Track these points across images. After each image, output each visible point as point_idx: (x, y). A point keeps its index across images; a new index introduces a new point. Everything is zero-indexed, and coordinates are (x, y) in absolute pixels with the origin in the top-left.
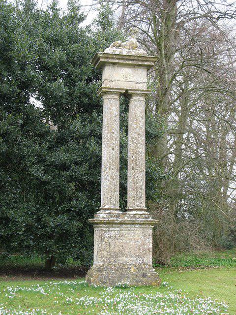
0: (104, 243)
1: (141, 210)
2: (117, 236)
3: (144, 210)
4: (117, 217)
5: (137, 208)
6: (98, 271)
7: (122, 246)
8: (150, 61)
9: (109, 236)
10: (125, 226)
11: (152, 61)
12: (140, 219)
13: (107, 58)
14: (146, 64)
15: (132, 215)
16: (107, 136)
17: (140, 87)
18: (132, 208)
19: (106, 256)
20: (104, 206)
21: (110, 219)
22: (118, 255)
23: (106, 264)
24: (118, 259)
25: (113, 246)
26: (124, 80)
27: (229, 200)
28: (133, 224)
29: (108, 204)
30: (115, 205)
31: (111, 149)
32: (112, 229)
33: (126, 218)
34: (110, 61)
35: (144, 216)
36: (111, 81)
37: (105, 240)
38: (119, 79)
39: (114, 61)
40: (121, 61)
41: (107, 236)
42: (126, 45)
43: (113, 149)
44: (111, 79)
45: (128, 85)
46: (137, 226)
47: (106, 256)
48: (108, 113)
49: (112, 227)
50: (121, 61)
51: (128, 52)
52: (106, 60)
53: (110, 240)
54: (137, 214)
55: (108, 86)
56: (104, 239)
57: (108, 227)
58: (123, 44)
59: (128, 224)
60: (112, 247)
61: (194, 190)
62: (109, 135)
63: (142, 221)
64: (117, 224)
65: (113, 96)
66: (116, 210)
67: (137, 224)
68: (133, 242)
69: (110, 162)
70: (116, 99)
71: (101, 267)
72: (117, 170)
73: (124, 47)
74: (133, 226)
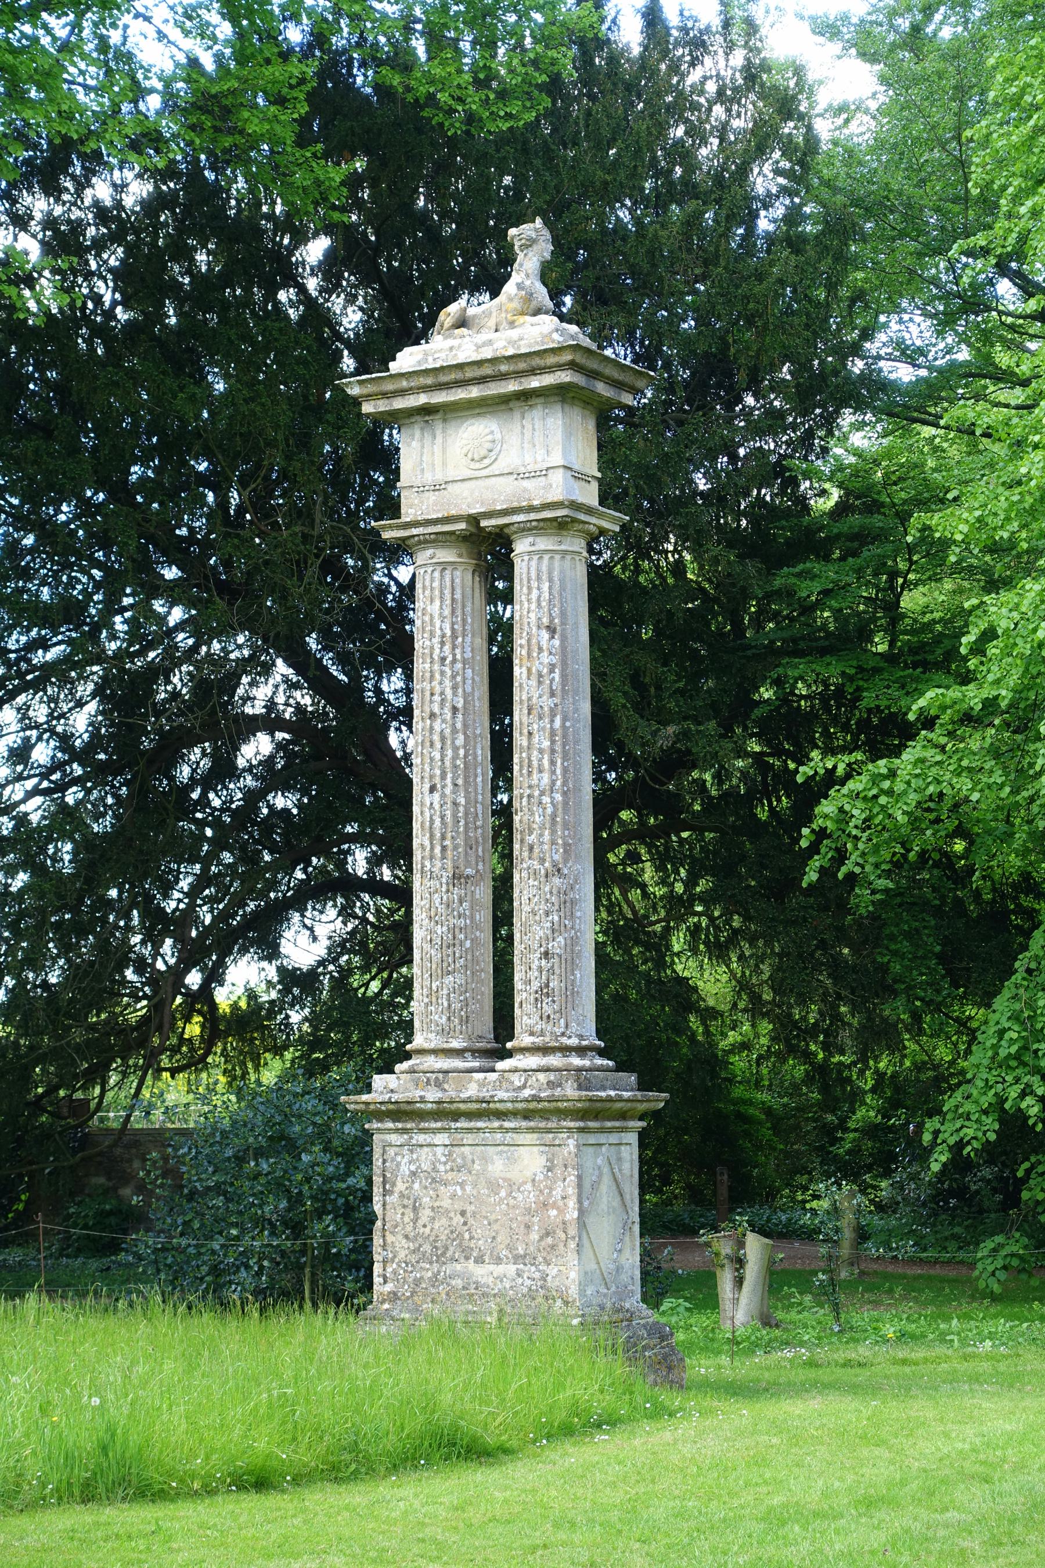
1: (581, 1051)
2: (442, 1168)
6: (928, 1529)
7: (463, 1213)
9: (413, 1168)
11: (560, 367)
17: (538, 492)
19: (402, 1255)
22: (449, 1254)
23: (406, 1290)
24: (449, 1269)
34: (399, 404)
35: (541, 1076)
36: (421, 490)
37: (400, 1186)
41: (405, 1170)
47: (402, 1255)
53: (416, 1186)
54: (515, 1070)
56: (394, 1185)
57: (405, 1131)
60: (425, 1214)
65: (429, 552)
68: (503, 1193)
70: (444, 566)
72: (457, 878)
74: (496, 1124)
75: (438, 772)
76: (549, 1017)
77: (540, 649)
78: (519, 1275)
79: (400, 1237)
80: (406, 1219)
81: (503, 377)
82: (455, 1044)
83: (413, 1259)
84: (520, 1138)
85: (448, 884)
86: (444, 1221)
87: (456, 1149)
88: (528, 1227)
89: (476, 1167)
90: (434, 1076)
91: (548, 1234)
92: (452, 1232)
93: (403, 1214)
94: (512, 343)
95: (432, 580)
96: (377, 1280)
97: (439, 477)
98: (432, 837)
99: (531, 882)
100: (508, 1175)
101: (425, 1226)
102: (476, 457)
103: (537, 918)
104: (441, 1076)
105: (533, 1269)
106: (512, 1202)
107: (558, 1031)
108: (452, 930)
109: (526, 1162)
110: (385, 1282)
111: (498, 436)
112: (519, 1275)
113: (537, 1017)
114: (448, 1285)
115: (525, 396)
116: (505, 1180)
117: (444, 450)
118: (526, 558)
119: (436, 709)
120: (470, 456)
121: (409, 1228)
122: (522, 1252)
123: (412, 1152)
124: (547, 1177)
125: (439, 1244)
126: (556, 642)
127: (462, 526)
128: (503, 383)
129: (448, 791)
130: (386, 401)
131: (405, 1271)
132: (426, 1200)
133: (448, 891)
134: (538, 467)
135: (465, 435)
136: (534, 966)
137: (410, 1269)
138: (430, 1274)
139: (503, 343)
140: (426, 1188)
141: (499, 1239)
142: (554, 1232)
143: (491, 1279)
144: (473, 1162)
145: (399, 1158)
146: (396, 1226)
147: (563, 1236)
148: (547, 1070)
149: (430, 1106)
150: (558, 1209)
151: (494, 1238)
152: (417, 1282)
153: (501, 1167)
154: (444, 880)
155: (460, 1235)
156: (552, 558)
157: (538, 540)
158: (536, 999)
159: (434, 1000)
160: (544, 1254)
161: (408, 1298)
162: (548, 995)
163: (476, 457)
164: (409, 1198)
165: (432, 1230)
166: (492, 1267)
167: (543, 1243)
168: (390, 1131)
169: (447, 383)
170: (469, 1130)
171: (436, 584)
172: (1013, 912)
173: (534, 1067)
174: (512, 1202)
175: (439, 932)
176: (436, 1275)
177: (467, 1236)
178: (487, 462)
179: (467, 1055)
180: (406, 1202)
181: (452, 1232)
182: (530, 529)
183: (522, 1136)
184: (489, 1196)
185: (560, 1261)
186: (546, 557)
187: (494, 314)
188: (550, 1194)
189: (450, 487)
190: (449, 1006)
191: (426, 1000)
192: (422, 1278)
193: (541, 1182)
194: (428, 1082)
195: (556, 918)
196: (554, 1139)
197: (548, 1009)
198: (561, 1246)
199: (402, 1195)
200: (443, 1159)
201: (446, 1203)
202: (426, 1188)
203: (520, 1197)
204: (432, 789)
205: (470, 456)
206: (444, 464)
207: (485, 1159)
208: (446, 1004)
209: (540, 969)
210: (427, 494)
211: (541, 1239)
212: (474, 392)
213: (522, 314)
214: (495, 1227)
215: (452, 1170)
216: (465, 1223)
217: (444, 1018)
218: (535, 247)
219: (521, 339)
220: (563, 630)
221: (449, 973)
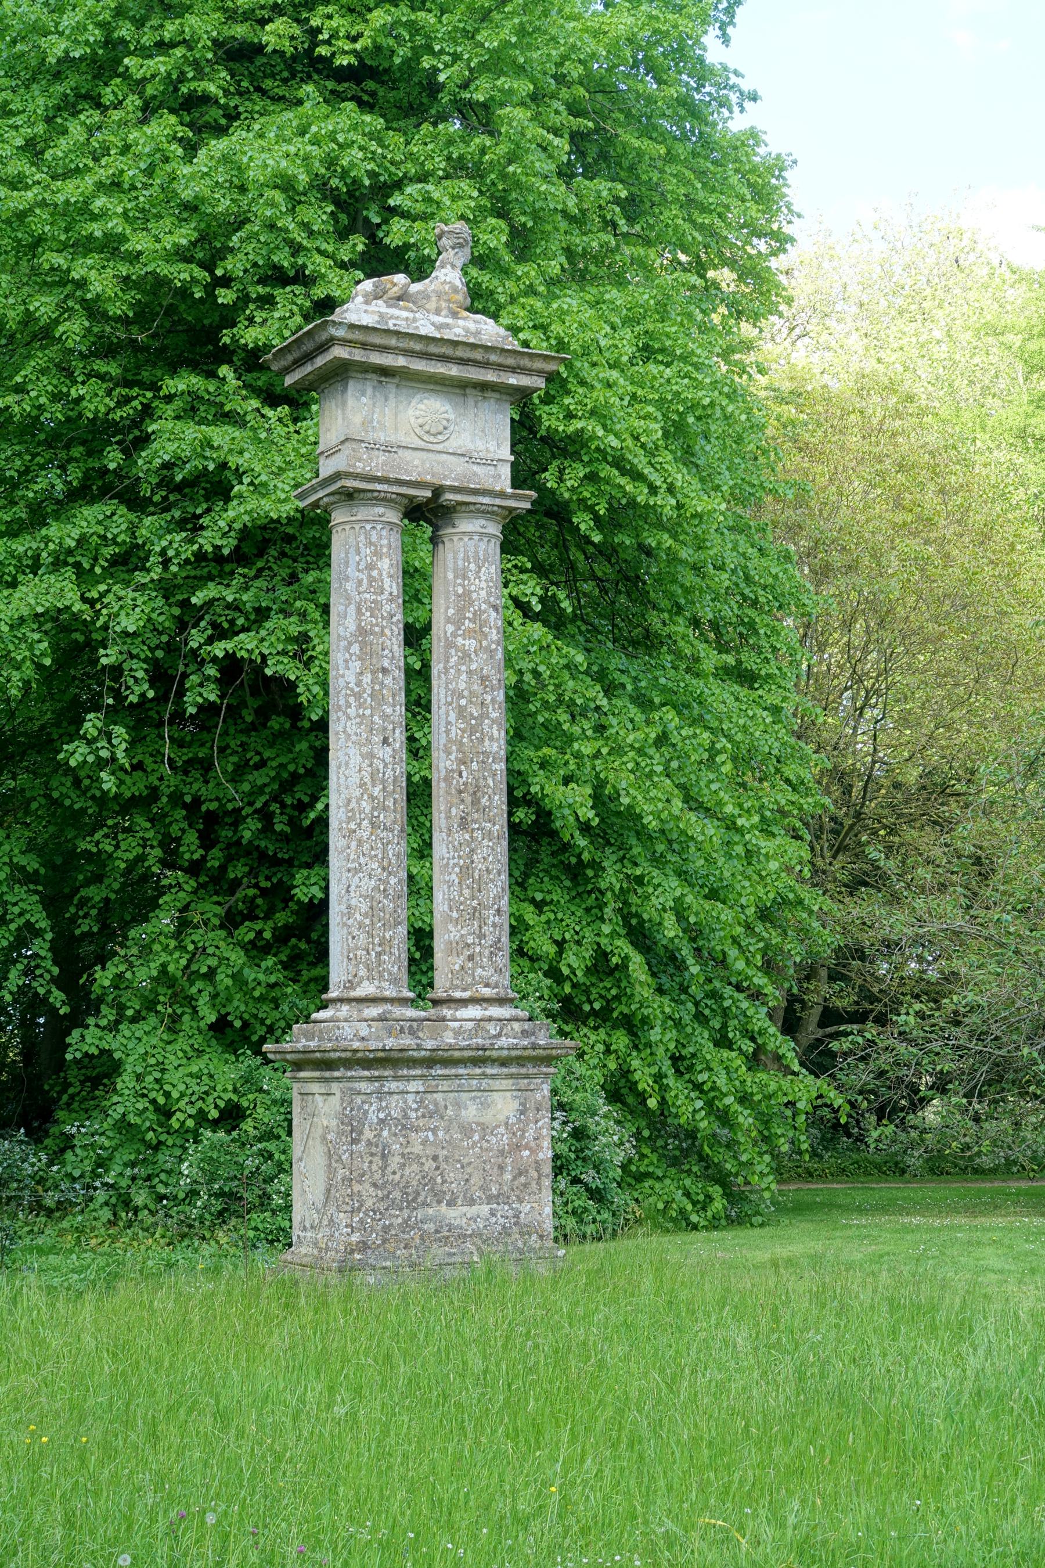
0: (361, 1147)
2: (413, 1115)
5: (487, 992)
7: (435, 1158)
9: (382, 1115)
10: (447, 1072)
11: (540, 373)
13: (364, 346)
14: (513, 380)
15: (470, 1025)
16: (359, 684)
18: (467, 995)
19: (369, 1203)
20: (351, 985)
21: (390, 1043)
24: (420, 1214)
25: (398, 1159)
26: (422, 444)
28: (477, 1062)
29: (370, 979)
30: (395, 981)
31: (377, 739)
33: (449, 1039)
34: (377, 359)
35: (516, 1026)
36: (373, 447)
37: (368, 1134)
38: (405, 440)
40: (419, 365)
43: (385, 741)
44: (370, 437)
45: (438, 469)
46: (489, 1071)
47: (369, 1203)
48: (360, 582)
49: (396, 1078)
50: (419, 365)
51: (439, 327)
52: (358, 355)
53: (385, 1133)
54: (490, 1019)
55: (359, 467)
56: (361, 1133)
58: (415, 287)
60: (395, 1162)
62: (367, 678)
63: (515, 1048)
64: (413, 1063)
65: (381, 510)
67: (493, 1061)
68: (476, 1137)
69: (372, 798)
71: (352, 1252)
74: (478, 1071)
78: (493, 1215)
79: (367, 1186)
80: (374, 1167)
81: (486, 365)
83: (382, 1206)
84: (496, 1084)
87: (428, 1096)
91: (520, 1174)
92: (423, 1177)
93: (371, 1162)
95: (380, 537)
97: (392, 439)
100: (482, 1120)
101: (394, 1173)
102: (433, 431)
104: (415, 1024)
105: (506, 1207)
106: (485, 1145)
112: (493, 1214)
114: (420, 1229)
115: (484, 387)
116: (478, 1124)
121: (377, 1176)
122: (494, 1192)
123: (381, 1100)
124: (519, 1120)
125: (409, 1190)
128: (482, 370)
130: (362, 352)
131: (373, 1219)
134: (490, 456)
138: (400, 1220)
140: (395, 1135)
142: (527, 1171)
144: (446, 1107)
145: (366, 1107)
146: (363, 1175)
147: (535, 1175)
149: (423, 1053)
150: (530, 1149)
151: (467, 1180)
152: (386, 1229)
153: (474, 1112)
155: (433, 1179)
160: (517, 1193)
161: (379, 1246)
164: (377, 1146)
166: (464, 1209)
170: (447, 1077)
171: (385, 542)
173: (508, 1017)
174: (485, 1145)
176: (406, 1221)
177: (439, 1180)
178: (441, 437)
180: (374, 1150)
181: (423, 1177)
183: (498, 1082)
184: (462, 1140)
185: (533, 1198)
188: (523, 1137)
189: (401, 452)
192: (391, 1225)
193: (513, 1124)
194: (402, 1031)
196: (529, 1084)
198: (534, 1184)
199: (369, 1143)
200: (414, 1106)
201: (417, 1149)
202: (395, 1135)
203: (494, 1140)
207: (458, 1105)
210: (376, 452)
211: (515, 1178)
214: (468, 1170)
215: (424, 1116)
216: (437, 1168)
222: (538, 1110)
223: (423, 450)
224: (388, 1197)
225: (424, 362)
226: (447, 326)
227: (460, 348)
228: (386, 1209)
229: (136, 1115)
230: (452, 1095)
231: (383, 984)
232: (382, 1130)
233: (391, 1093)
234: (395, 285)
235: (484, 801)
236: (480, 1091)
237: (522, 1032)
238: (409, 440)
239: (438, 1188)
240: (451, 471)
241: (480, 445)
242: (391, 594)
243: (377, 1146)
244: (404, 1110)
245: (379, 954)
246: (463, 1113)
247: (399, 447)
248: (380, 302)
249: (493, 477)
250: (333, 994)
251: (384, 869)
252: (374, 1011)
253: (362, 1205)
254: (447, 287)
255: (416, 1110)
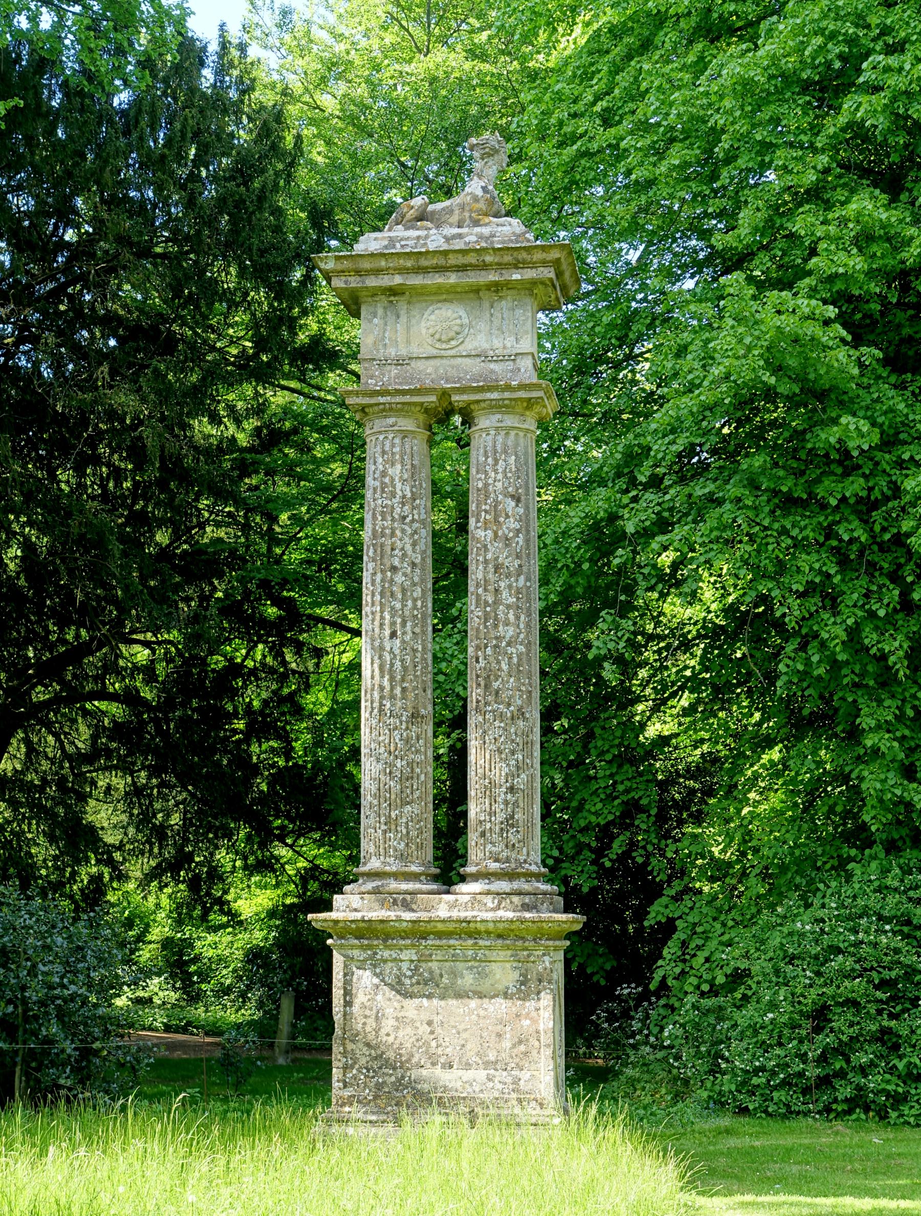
2: (408, 981)
3: (529, 876)
4: (407, 906)
5: (494, 866)
7: (430, 1023)
8: (533, 265)
10: (438, 942)
11: (544, 263)
12: (501, 913)
14: (516, 276)
15: (467, 898)
26: (435, 352)
27: (294, 284)
32: (386, 954)
33: (443, 912)
34: (372, 282)
35: (515, 899)
36: (384, 363)
38: (415, 350)
39: (385, 281)
40: (416, 280)
42: (450, 211)
45: (453, 373)
46: (481, 942)
47: (363, 1061)
51: (448, 239)
57: (369, 947)
59: (449, 935)
61: (24, 447)
62: (379, 577)
65: (391, 421)
66: (414, 877)
70: (404, 434)
72: (415, 716)
73: (437, 220)
74: (470, 942)
75: (399, 620)
76: (514, 845)
77: (507, 516)
78: (489, 1080)
79: (360, 1045)
81: (484, 267)
82: (414, 868)
84: (493, 955)
85: (407, 722)
86: (409, 1030)
87: (424, 965)
88: (499, 1035)
89: (445, 980)
90: (401, 897)
91: (520, 1042)
92: (418, 1040)
94: (481, 237)
95: (393, 445)
96: (336, 1085)
97: (403, 352)
98: (392, 679)
99: (497, 723)
101: (388, 1035)
102: (444, 338)
103: (503, 756)
104: (408, 897)
105: (505, 1073)
106: (482, 1013)
107: (522, 858)
108: (410, 764)
109: (498, 976)
110: (345, 1087)
111: (466, 321)
112: (490, 1079)
113: (502, 846)
114: (413, 1089)
115: (496, 288)
117: (408, 329)
118: (493, 432)
119: (396, 563)
120: (437, 336)
122: (492, 1059)
125: (403, 1051)
126: (521, 511)
127: (433, 398)
128: (483, 273)
129: (408, 638)
130: (358, 279)
131: (366, 1076)
132: (389, 1011)
133: (407, 728)
134: (506, 352)
135: (433, 317)
136: (499, 800)
137: (371, 1074)
138: (393, 1079)
139: (474, 238)
140: (390, 999)
141: (468, 1047)
142: (527, 1040)
143: (459, 1083)
144: (441, 976)
147: (537, 1043)
148: (519, 893)
149: (405, 924)
151: (463, 1046)
152: (379, 1086)
153: (471, 981)
154: (404, 719)
155: (427, 1044)
156: (507, 434)
157: (506, 417)
158: (502, 829)
159: (393, 827)
162: (512, 826)
163: (444, 338)
164: (371, 1009)
165: (396, 1038)
166: (460, 1072)
167: (515, 1050)
168: (352, 947)
169: (427, 268)
171: (397, 449)
172: (671, 807)
173: (508, 890)
174: (482, 1013)
175: (399, 765)
177: (434, 1044)
178: (453, 343)
179: (423, 878)
180: (368, 1012)
181: (418, 1040)
182: (501, 407)
185: (533, 1067)
186: (513, 433)
187: (457, 212)
189: (413, 363)
190: (408, 833)
191: (383, 827)
192: (385, 1082)
194: (395, 901)
195: (521, 757)
196: (529, 956)
197: (513, 839)
198: (534, 1052)
200: (409, 973)
202: (390, 999)
204: (393, 635)
205: (437, 336)
206: (408, 342)
207: (454, 974)
208: (404, 831)
209: (506, 803)
210: (389, 367)
211: (514, 1046)
212: (453, 279)
213: (486, 215)
214: (465, 1035)
215: (418, 983)
216: (432, 1032)
217: (403, 844)
218: (496, 157)
219: (494, 236)
220: (527, 500)
221: (408, 803)
222: (540, 981)
223: (435, 357)
224: (381, 1056)
225: (421, 277)
226: (460, 236)
227: (451, 256)
228: (380, 1068)
229: (674, 978)
230: (447, 964)
231: (388, 859)
232: (376, 994)
233: (385, 961)
234: (412, 207)
235: (496, 685)
236: (475, 959)
237: (522, 905)
238: (421, 350)
239: (432, 1051)
240: (467, 373)
241: (497, 343)
242: (404, 497)
243: (371, 1009)
244: (398, 977)
245: (385, 832)
246: (459, 982)
247: (410, 358)
248: (400, 227)
249: (512, 371)
250: (470, 869)
251: (390, 753)
252: (370, 886)
253: (355, 1063)
254: (469, 198)
255: (411, 977)
